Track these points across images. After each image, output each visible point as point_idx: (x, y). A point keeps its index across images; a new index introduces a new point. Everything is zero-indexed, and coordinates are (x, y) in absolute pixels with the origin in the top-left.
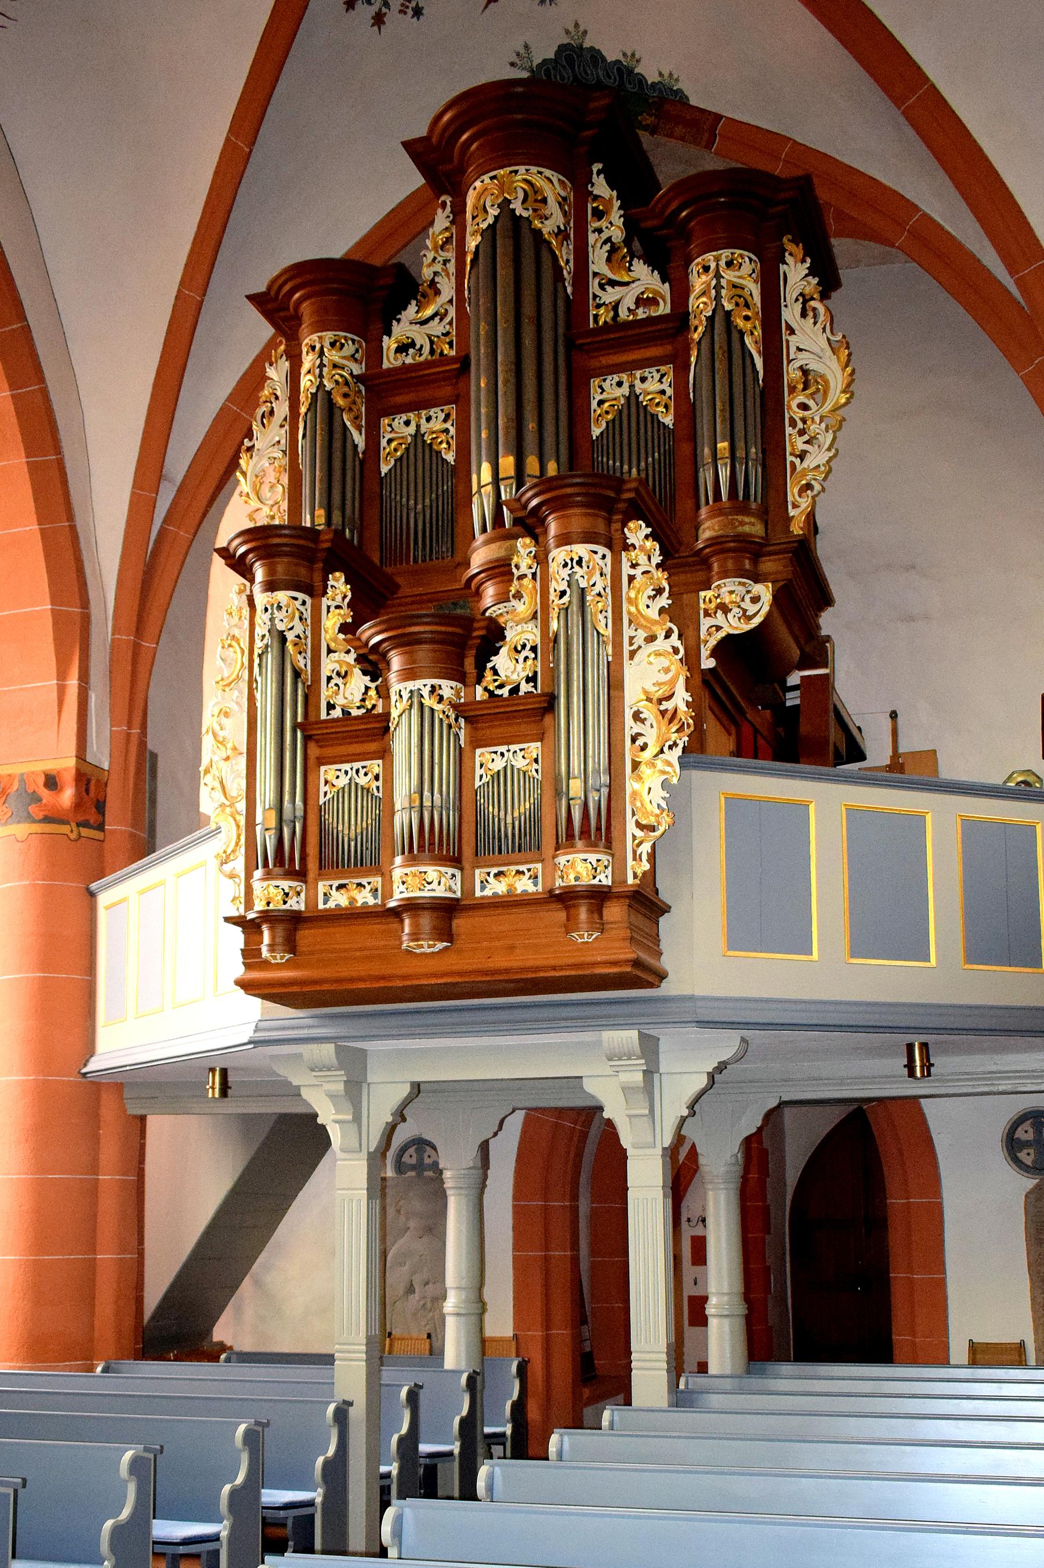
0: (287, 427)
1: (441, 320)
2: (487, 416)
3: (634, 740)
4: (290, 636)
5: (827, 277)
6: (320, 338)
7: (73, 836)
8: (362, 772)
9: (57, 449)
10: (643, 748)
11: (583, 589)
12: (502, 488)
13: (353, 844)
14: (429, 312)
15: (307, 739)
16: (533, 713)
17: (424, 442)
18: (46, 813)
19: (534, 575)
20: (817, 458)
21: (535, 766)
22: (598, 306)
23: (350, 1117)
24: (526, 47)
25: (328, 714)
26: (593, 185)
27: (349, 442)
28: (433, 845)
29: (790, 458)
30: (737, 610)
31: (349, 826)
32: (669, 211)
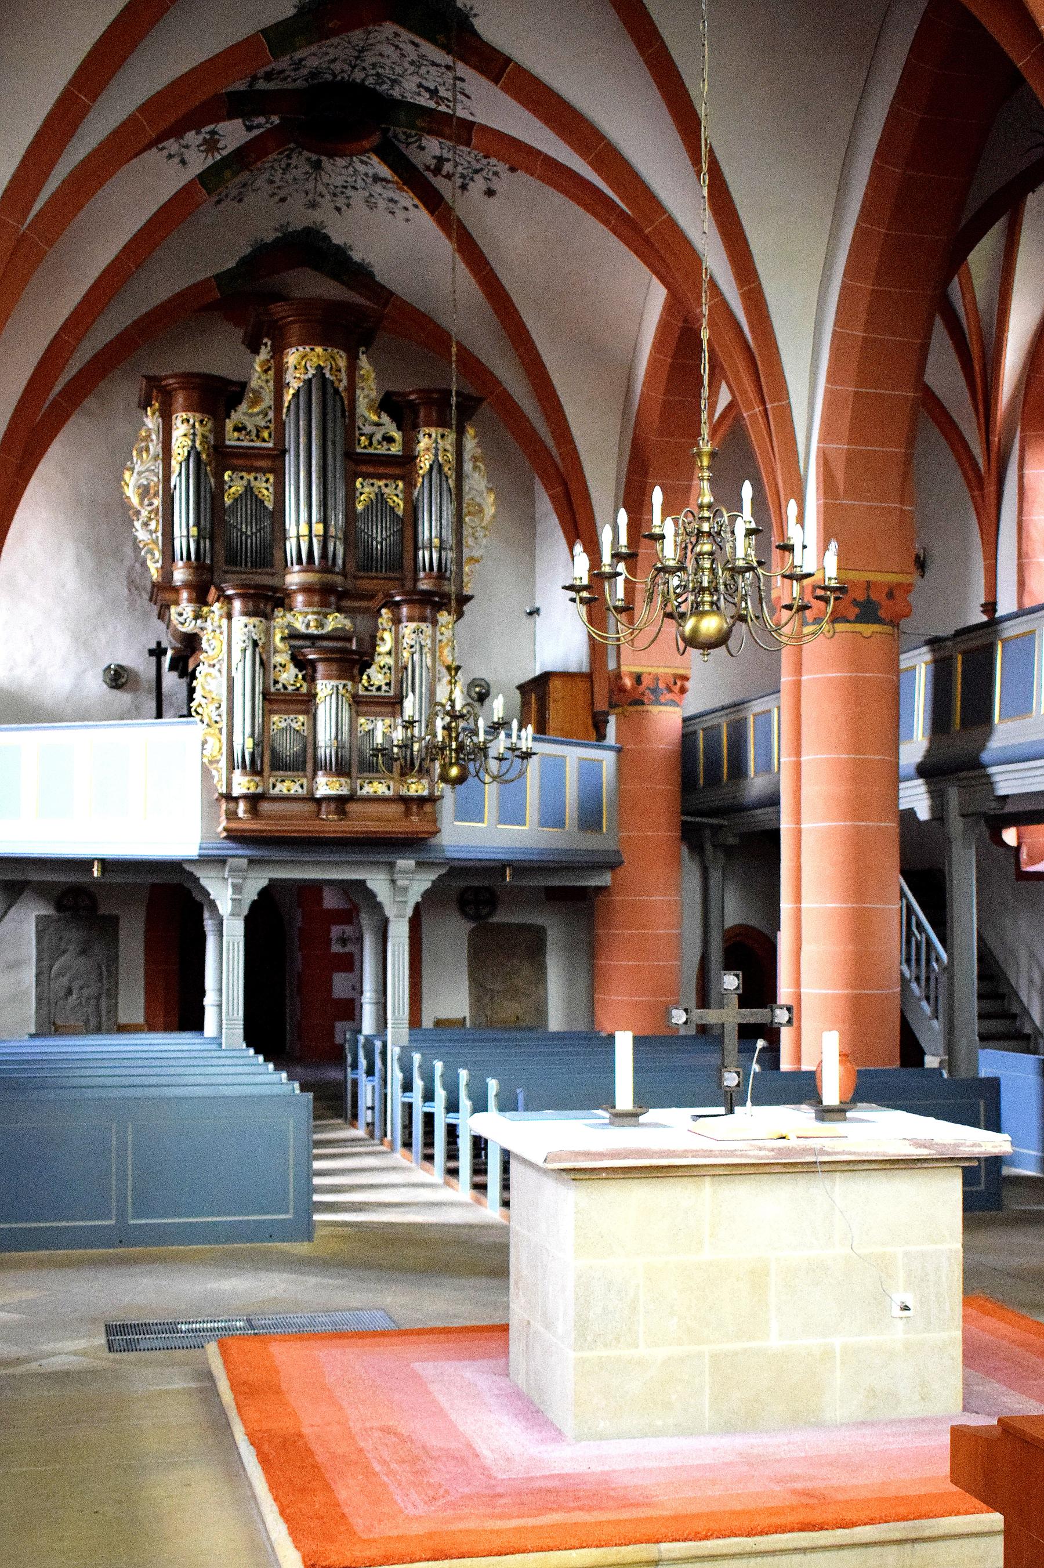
4: (260, 643)
22: (362, 435)
28: (341, 768)
31: (289, 747)
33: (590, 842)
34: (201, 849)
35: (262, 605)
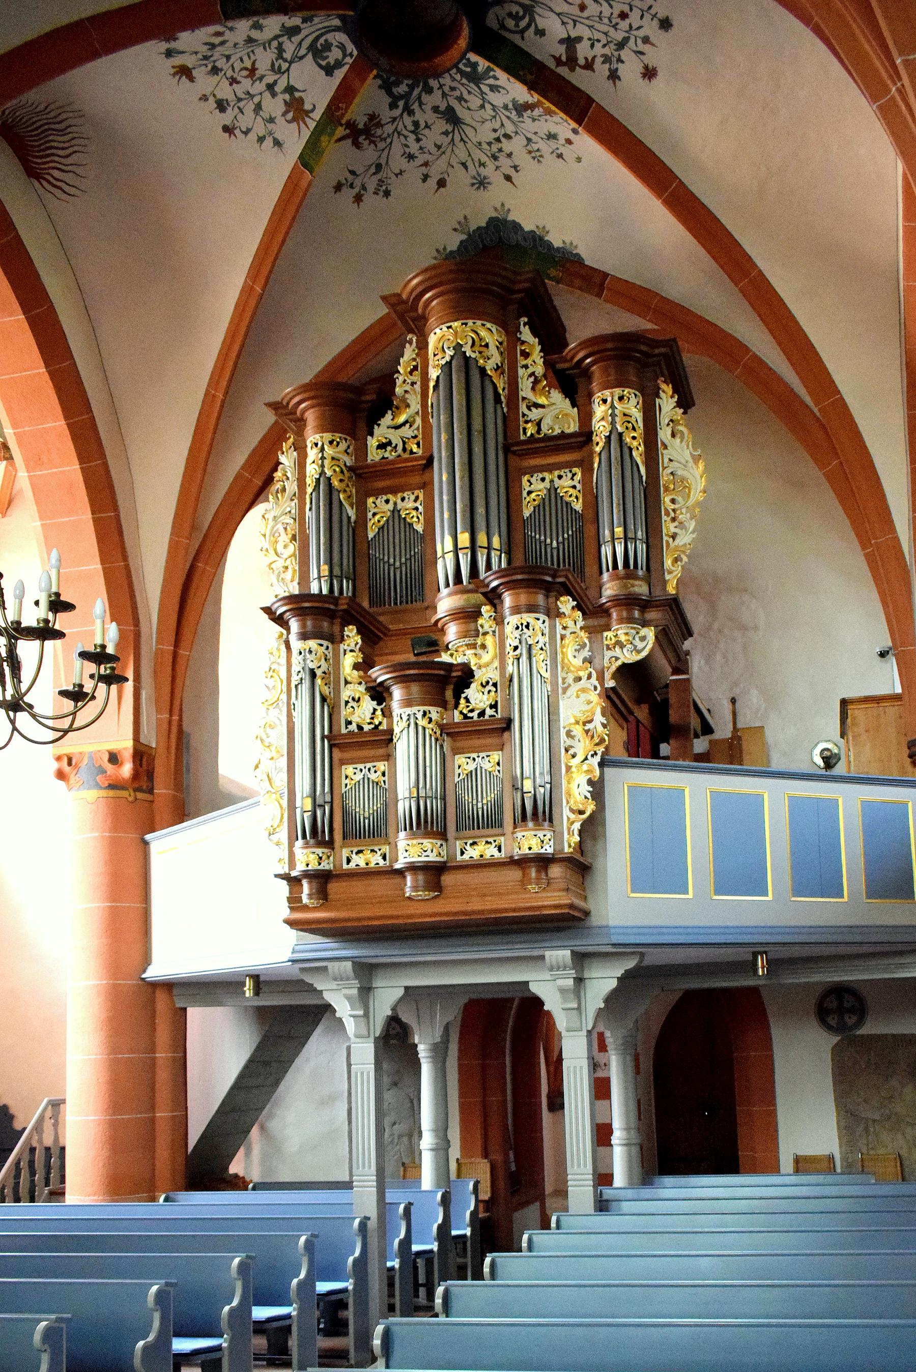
0: (296, 501)
1: (411, 426)
2: (448, 501)
3: (567, 750)
4: (319, 672)
5: (685, 403)
6: (322, 437)
7: (131, 799)
8: (373, 770)
9: (115, 508)
10: (574, 756)
11: (530, 645)
12: (460, 555)
13: (367, 821)
14: (402, 419)
15: (331, 746)
16: (497, 729)
17: (400, 516)
18: (111, 782)
19: (494, 632)
20: (684, 539)
21: (498, 768)
22: (527, 422)
23: (361, 1013)
24: (465, 218)
25: (347, 728)
26: (521, 333)
27: (344, 515)
28: (427, 824)
29: (665, 538)
30: (630, 646)
31: (364, 808)
32: (576, 360)
33: (893, 914)
34: (294, 952)
35: (325, 624)
